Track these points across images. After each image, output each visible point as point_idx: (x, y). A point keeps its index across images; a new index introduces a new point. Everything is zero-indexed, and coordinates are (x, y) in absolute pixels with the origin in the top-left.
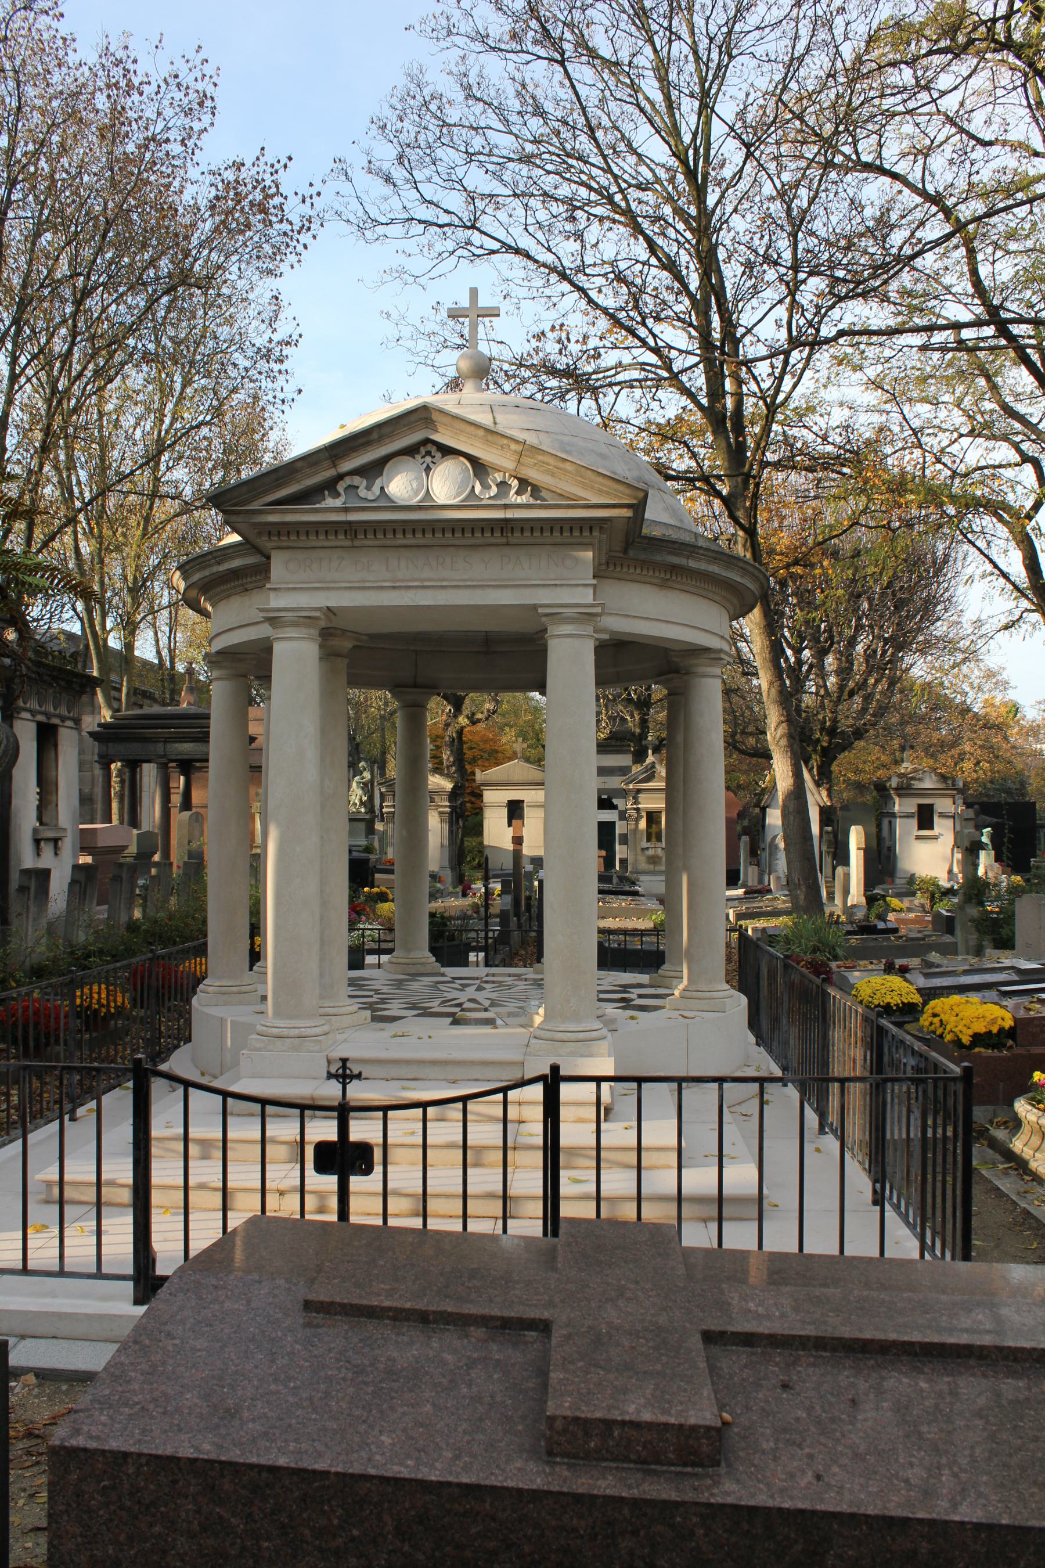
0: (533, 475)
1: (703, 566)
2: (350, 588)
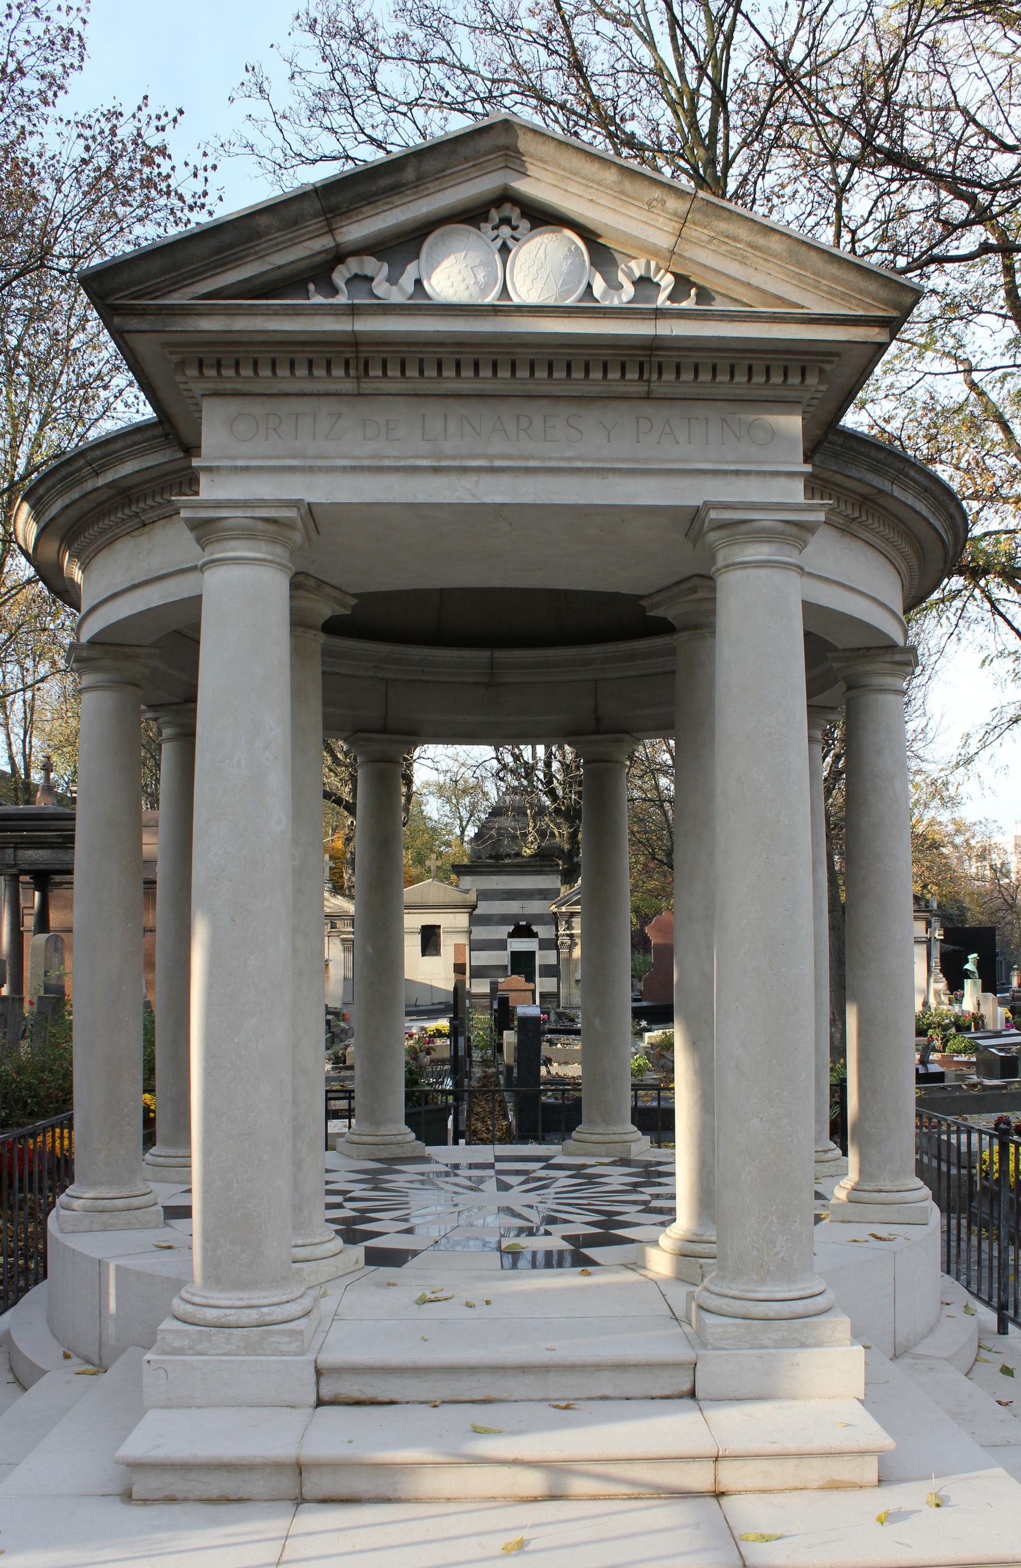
2: (353, 469)
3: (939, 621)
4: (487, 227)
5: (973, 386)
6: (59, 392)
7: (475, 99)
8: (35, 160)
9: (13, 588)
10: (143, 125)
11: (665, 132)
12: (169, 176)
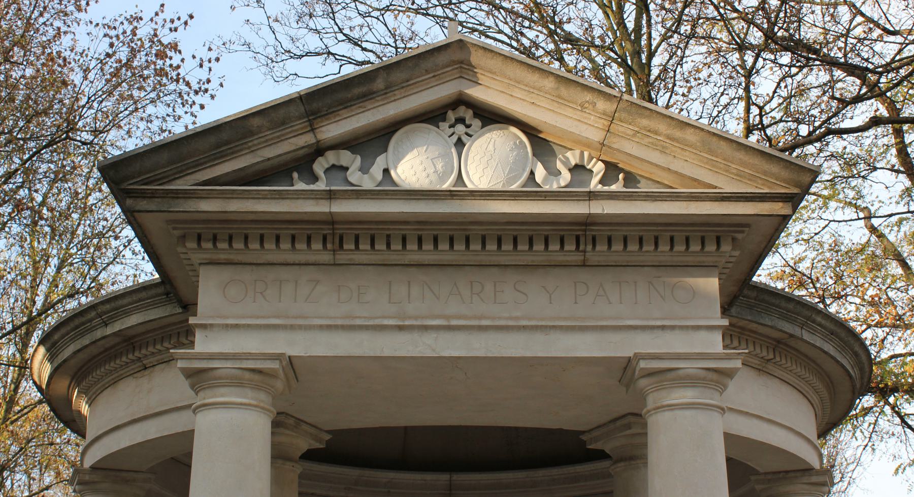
2: (329, 327)
3: (854, 434)
4: (444, 125)
5: (873, 230)
6: (76, 241)
7: (436, 6)
8: (66, 54)
9: (25, 408)
10: (159, 27)
11: (597, 32)
12: (178, 67)
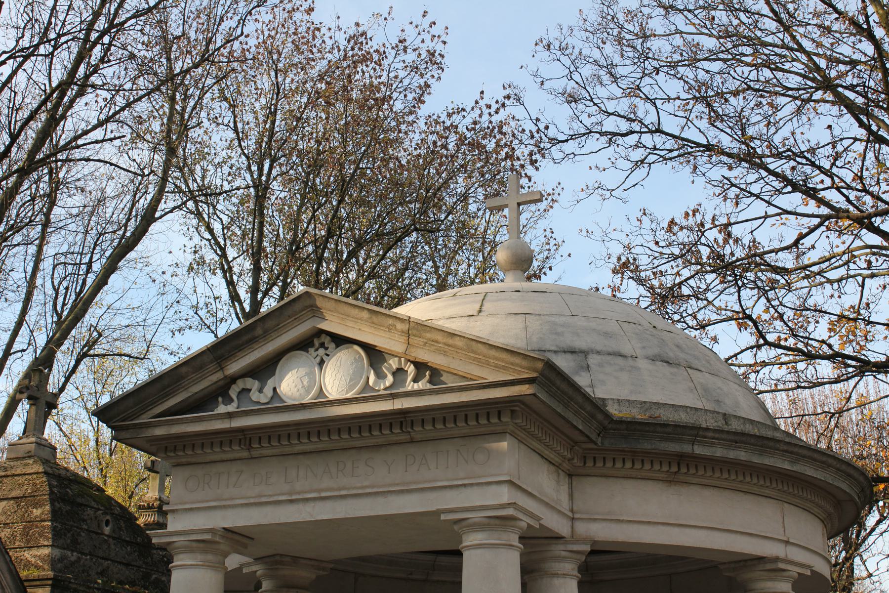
0: (423, 356)
1: (719, 452)
2: (247, 505)
4: (312, 350)
